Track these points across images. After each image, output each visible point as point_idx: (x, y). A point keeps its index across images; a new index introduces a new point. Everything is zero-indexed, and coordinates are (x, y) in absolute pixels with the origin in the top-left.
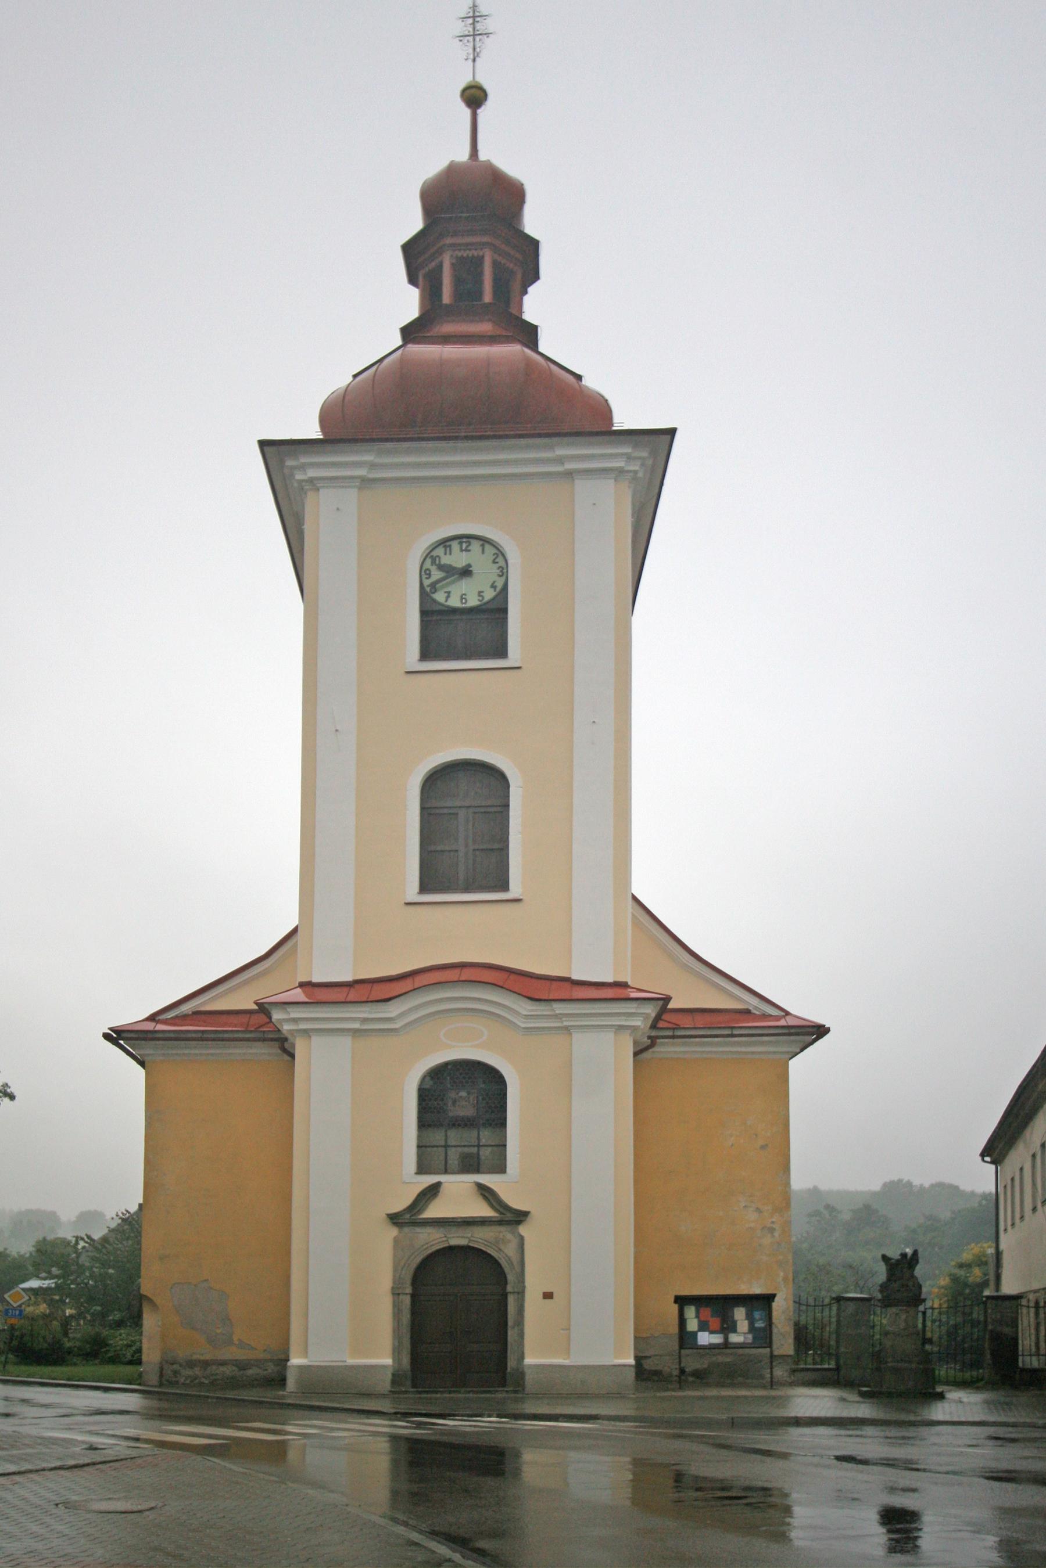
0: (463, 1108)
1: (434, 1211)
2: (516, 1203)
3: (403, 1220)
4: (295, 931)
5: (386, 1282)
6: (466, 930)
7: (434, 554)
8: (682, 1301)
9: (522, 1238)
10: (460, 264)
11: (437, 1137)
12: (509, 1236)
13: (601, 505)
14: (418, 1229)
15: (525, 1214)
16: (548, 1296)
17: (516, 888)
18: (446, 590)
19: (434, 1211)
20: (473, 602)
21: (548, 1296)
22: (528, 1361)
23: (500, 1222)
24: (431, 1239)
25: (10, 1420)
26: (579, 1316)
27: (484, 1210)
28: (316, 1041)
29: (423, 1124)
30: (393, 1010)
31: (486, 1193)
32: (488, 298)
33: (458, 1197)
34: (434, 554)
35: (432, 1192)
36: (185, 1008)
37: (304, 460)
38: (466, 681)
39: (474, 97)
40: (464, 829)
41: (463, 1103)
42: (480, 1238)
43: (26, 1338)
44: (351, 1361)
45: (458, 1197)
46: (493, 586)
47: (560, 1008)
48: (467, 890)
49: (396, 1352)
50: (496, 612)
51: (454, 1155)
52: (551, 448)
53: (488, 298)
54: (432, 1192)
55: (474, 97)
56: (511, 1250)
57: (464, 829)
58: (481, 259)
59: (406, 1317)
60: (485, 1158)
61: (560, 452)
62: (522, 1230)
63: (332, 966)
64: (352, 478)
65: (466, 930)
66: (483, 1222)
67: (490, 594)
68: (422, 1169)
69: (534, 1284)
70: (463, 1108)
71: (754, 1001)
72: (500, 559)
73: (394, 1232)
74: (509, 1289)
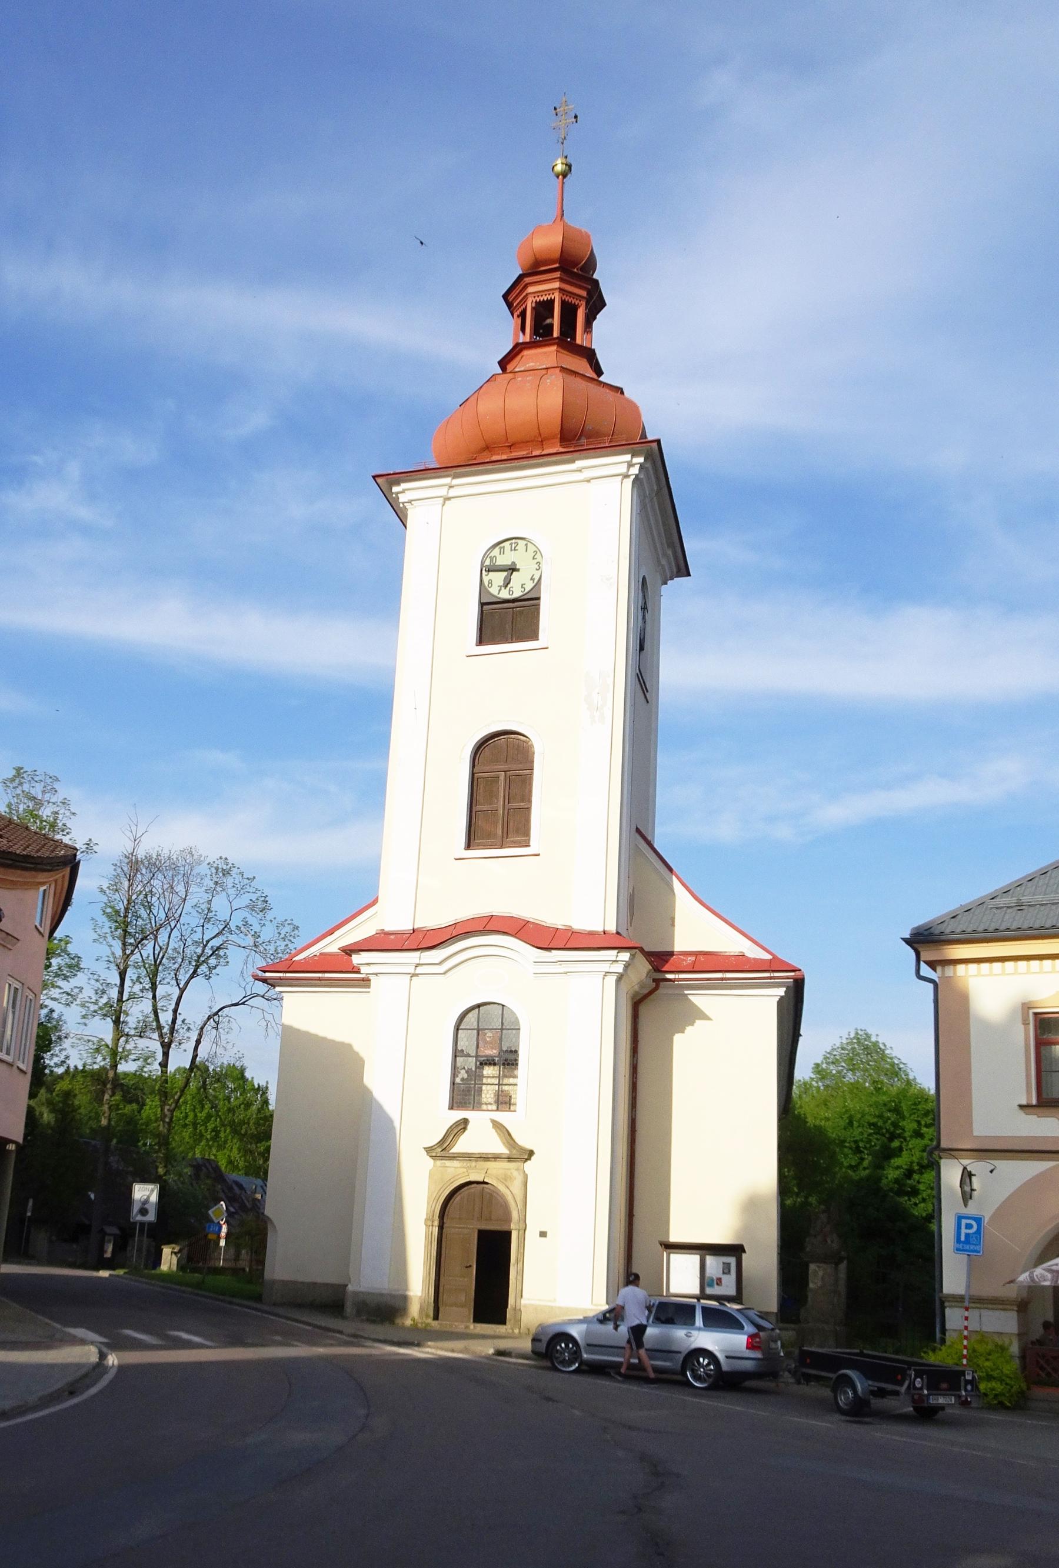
0: (485, 1057)
1: (459, 1148)
2: (524, 1141)
6: (498, 882)
7: (492, 554)
9: (526, 1176)
10: (651, 1358)
12: (515, 1174)
14: (448, 1163)
16: (543, 1234)
18: (435, 1324)
19: (462, 1145)
21: (543, 1234)
23: (510, 1159)
24: (458, 1173)
32: (556, 334)
33: (480, 1135)
34: (492, 554)
37: (404, 486)
38: (509, 656)
42: (492, 1173)
43: (152, 1107)
46: (532, 579)
52: (573, 461)
53: (556, 334)
58: (552, 301)
61: (579, 464)
65: (498, 882)
66: (496, 1157)
67: (529, 586)
68: (455, 1103)
72: (538, 556)
74: (513, 1226)
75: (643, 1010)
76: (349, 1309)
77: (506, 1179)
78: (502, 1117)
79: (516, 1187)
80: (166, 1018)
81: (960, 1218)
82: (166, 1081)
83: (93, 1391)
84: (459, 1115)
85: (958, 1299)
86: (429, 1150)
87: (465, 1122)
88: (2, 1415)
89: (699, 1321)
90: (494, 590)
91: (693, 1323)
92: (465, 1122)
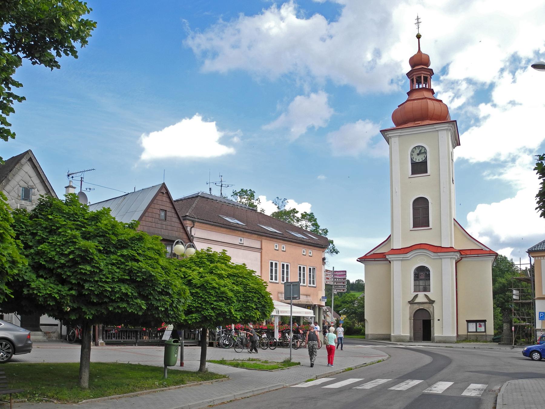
0: (422, 275)
1: (417, 300)
2: (432, 299)
3: (412, 302)
4: (390, 236)
5: (408, 317)
6: (422, 236)
8: (468, 321)
11: (417, 282)
13: (445, 137)
15: (434, 301)
16: (439, 320)
17: (431, 226)
19: (417, 300)
20: (421, 161)
21: (439, 320)
22: (435, 335)
23: (430, 303)
24: (417, 307)
25: (293, 370)
26: (444, 327)
27: (425, 300)
28: (395, 262)
29: (415, 280)
30: (408, 255)
31: (426, 296)
33: (421, 298)
35: (416, 296)
36: (372, 253)
38: (420, 178)
39: (419, 37)
40: (421, 212)
41: (422, 275)
42: (425, 307)
44: (402, 334)
45: (421, 298)
47: (439, 254)
48: (422, 227)
49: (410, 332)
50: (425, 163)
51: (421, 287)
54: (416, 296)
55: (419, 37)
56: (431, 310)
57: (421, 212)
58: (421, 77)
59: (412, 324)
60: (426, 289)
62: (434, 305)
63: (397, 245)
64: (437, 342)
65: (422, 236)
69: (436, 317)
70: (422, 275)
71: (483, 247)
73: (410, 305)
75: (458, 264)
76: (392, 339)
77: (429, 308)
78: (426, 293)
79: (431, 310)
80: (340, 346)
81: (540, 313)
82: (372, 68)
83: (227, 219)
84: (416, 293)
85: (540, 330)
86: (409, 302)
87: (417, 295)
88: (543, 256)
89: (85, 382)
90: (414, 160)
91: (79, 383)
92: (417, 295)
